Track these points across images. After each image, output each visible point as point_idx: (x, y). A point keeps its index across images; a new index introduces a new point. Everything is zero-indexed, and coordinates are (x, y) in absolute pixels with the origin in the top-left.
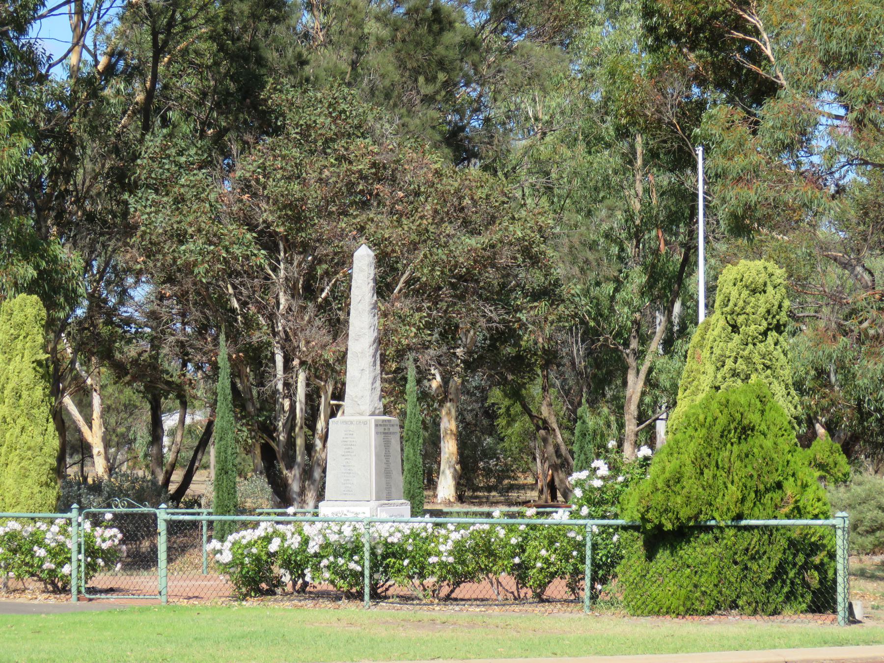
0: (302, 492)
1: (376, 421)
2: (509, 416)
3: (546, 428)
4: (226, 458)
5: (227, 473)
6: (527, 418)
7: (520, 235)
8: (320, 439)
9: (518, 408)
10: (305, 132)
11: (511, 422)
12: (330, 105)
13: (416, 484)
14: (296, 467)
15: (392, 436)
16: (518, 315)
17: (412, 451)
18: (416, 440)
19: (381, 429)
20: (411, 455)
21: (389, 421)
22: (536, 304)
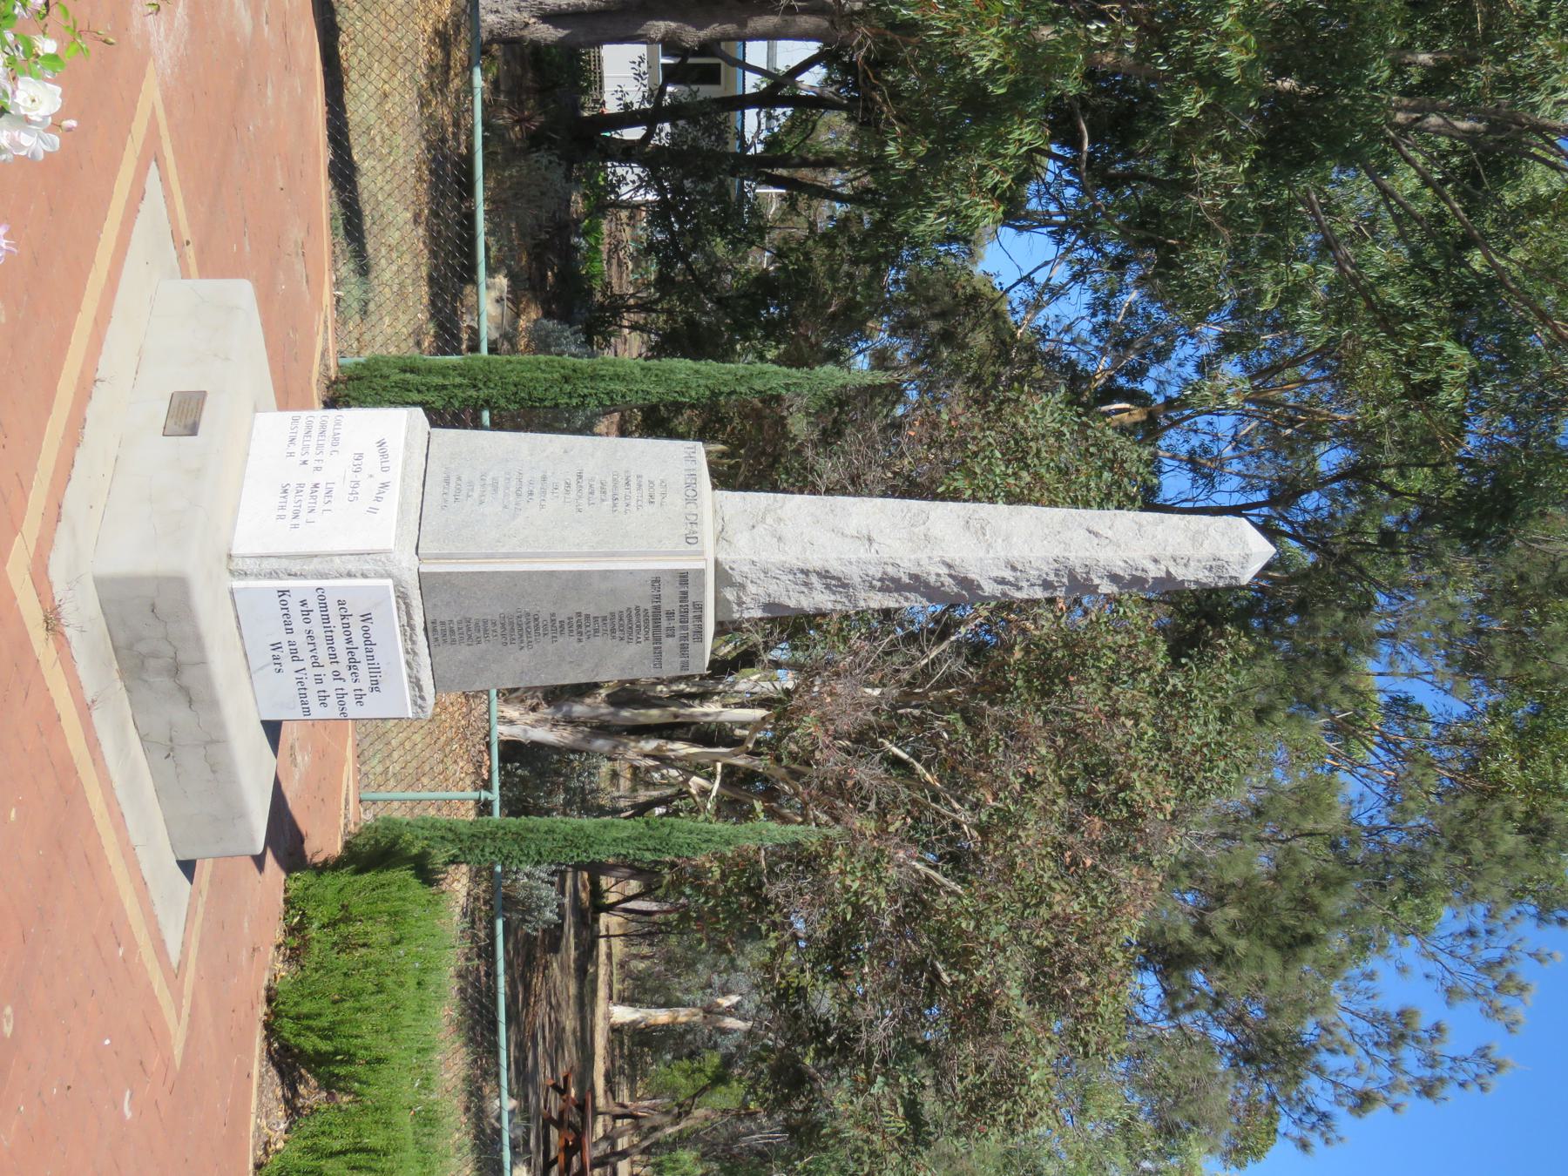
0: (571, 721)
1: (701, 572)
2: (693, 1072)
3: (680, 1114)
4: (602, 378)
5: (566, 379)
6: (691, 1092)
7: (1033, 1078)
8: (658, 748)
9: (704, 1081)
10: (1181, 698)
11: (688, 1075)
12: (1221, 745)
13: (549, 845)
14: (612, 709)
15: (647, 646)
16: (880, 1079)
17: (624, 834)
18: (651, 844)
19: (670, 601)
20: (615, 834)
21: (699, 634)
22: (901, 1110)
